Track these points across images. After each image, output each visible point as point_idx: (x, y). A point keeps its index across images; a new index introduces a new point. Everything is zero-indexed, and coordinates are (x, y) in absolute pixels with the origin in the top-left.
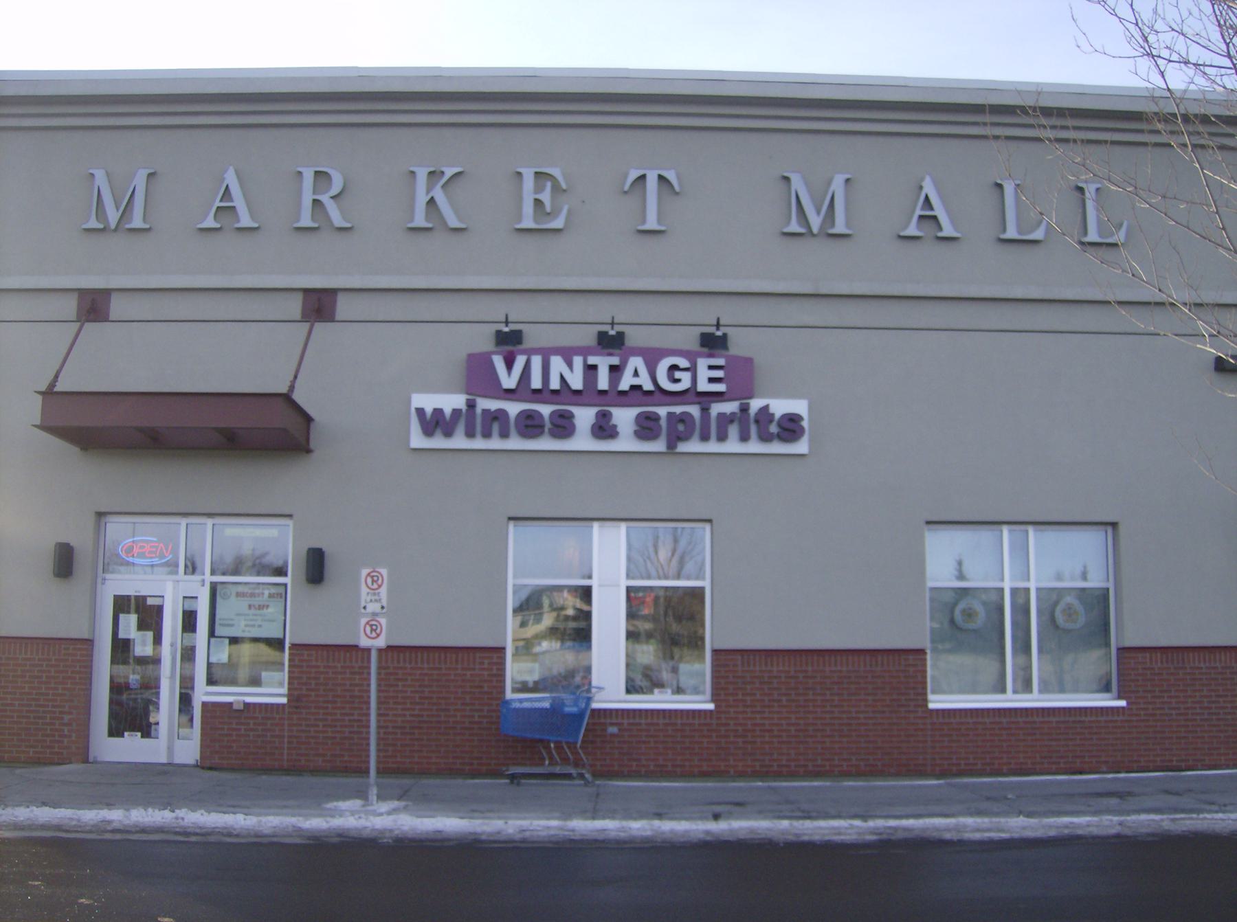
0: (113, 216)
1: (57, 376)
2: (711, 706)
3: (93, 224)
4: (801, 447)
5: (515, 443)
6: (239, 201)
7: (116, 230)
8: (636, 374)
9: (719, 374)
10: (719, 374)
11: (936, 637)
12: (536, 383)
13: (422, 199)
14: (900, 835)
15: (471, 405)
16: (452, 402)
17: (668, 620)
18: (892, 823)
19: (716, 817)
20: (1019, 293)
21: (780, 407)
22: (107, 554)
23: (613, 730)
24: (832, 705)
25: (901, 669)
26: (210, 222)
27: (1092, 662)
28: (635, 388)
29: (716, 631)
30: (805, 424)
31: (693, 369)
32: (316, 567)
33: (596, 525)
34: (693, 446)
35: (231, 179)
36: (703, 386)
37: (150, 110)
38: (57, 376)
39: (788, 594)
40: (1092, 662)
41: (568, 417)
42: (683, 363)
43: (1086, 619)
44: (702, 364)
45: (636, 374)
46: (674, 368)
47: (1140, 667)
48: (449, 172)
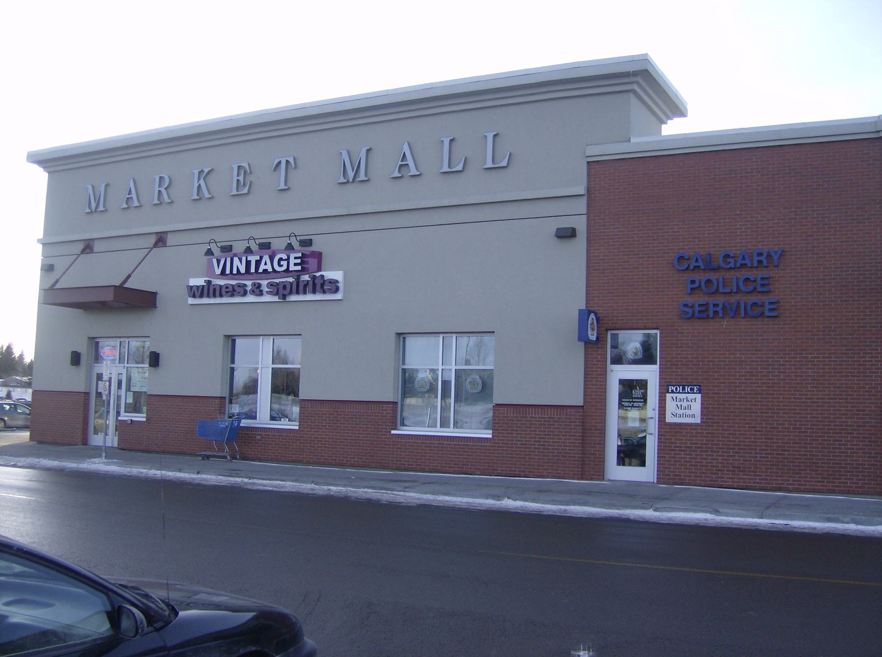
0: (351, 174)
1: (129, 276)
2: (488, 434)
3: (342, 180)
4: (338, 296)
5: (251, 298)
6: (410, 161)
7: (96, 211)
8: (266, 264)
9: (299, 261)
10: (299, 261)
11: (134, 392)
12: (228, 272)
13: (196, 185)
14: (446, 504)
15: (209, 282)
16: (200, 282)
17: (286, 384)
18: (430, 497)
19: (198, 473)
20: (446, 203)
21: (329, 275)
22: (131, 352)
23: (258, 437)
24: (358, 431)
25: (388, 413)
26: (397, 174)
27: (481, 410)
28: (265, 271)
29: (306, 391)
30: (341, 285)
31: (288, 260)
32: (155, 360)
33: (261, 338)
34: (293, 298)
35: (406, 149)
36: (292, 268)
37: (386, 112)
38: (129, 276)
39: (343, 375)
40: (481, 410)
41: (260, 285)
42: (285, 257)
43: (474, 387)
44: (292, 256)
45: (266, 264)
46: (281, 259)
47: (507, 416)
48: (206, 170)
